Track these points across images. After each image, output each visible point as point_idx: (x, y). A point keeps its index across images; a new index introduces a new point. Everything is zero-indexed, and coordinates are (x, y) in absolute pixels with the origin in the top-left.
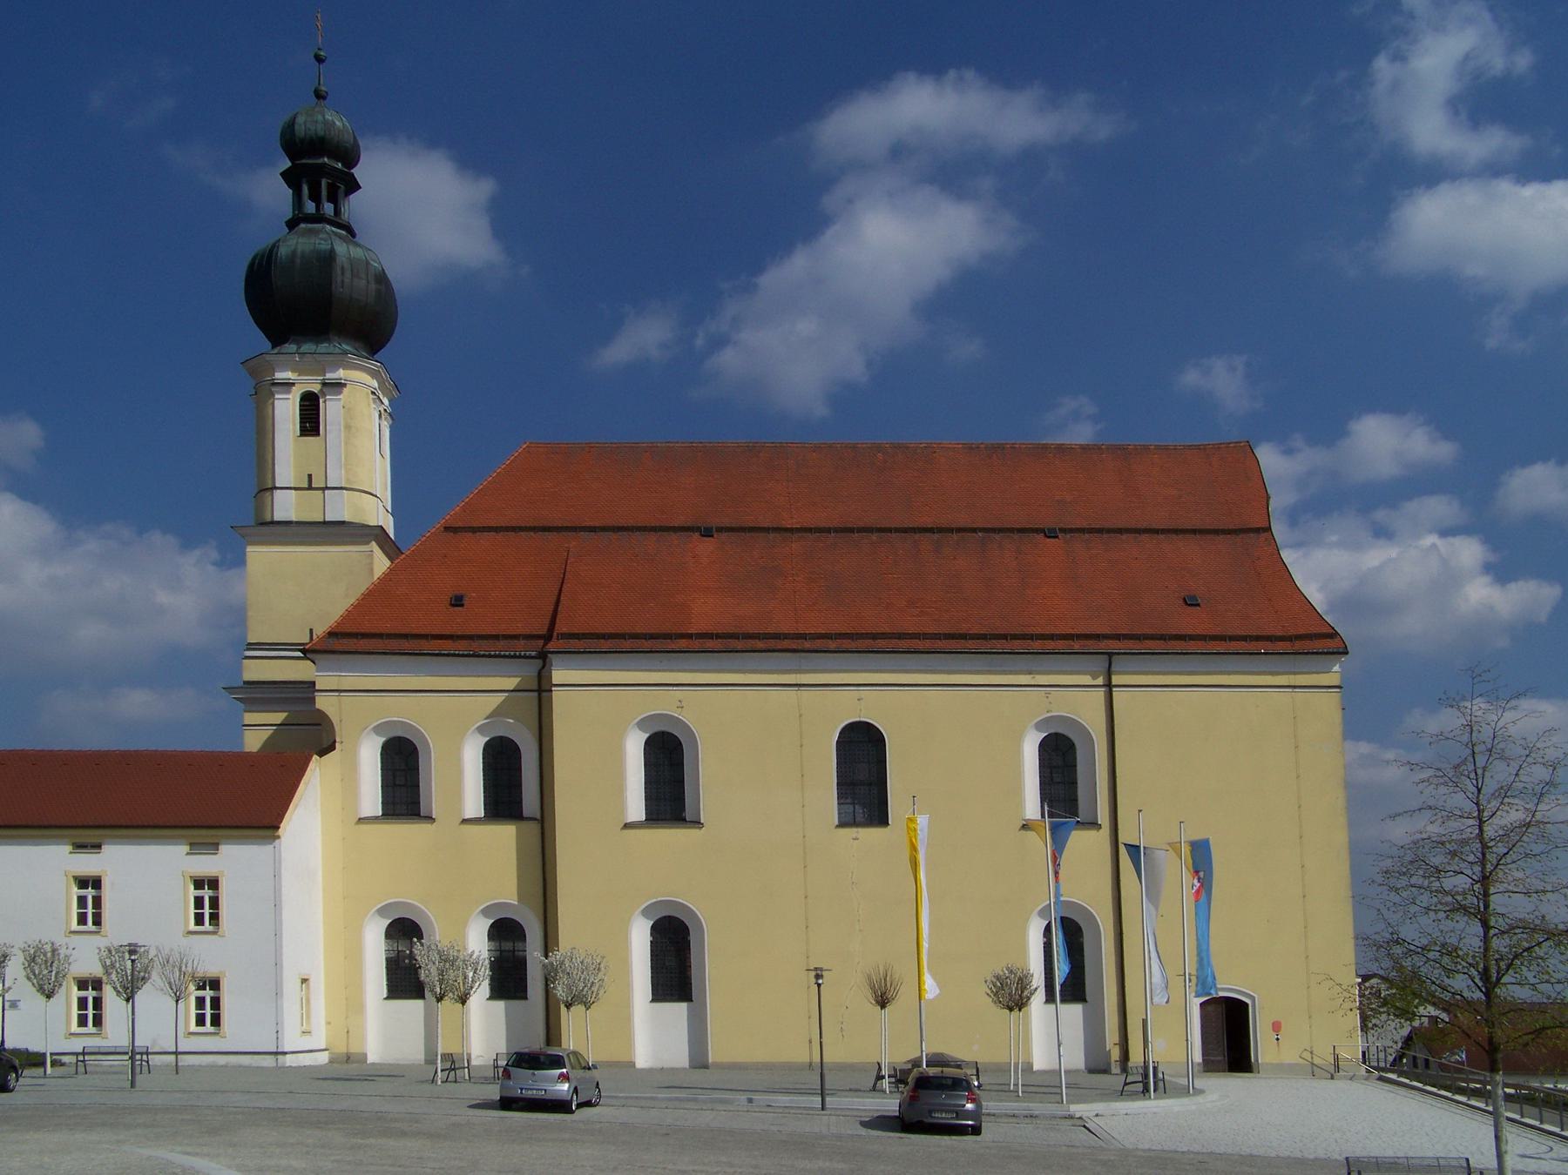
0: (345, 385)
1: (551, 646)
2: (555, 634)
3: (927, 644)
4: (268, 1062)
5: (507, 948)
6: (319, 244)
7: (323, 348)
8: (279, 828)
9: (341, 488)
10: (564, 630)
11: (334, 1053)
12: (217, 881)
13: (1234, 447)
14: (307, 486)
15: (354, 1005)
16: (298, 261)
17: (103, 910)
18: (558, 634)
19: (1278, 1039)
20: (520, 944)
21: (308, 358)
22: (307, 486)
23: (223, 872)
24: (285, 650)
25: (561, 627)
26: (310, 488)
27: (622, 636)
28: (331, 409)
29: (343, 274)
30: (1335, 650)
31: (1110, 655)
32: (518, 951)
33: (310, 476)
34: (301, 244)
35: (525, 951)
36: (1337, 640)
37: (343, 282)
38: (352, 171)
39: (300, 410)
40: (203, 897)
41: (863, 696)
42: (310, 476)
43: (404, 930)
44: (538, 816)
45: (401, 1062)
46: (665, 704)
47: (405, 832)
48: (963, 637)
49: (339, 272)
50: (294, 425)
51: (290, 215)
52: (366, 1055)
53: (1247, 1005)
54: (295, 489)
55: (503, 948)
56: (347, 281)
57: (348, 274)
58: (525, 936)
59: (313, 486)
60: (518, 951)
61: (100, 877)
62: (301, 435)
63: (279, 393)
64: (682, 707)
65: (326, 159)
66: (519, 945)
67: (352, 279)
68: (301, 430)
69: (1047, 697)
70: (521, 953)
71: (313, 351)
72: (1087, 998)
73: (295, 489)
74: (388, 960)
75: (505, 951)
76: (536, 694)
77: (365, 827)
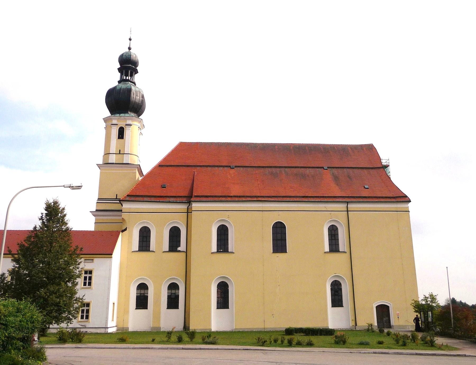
0: (132, 125)
1: (192, 199)
2: (193, 196)
3: (300, 199)
4: (102, 331)
5: (173, 292)
6: (128, 87)
7: (127, 115)
8: (112, 254)
9: (128, 154)
10: (196, 195)
11: (118, 328)
12: (92, 271)
13: (240, 145)
14: (119, 153)
15: (126, 312)
16: (121, 91)
17: (92, 281)
18: (194, 196)
19: (398, 317)
20: (177, 291)
21: (122, 118)
22: (119, 153)
23: (94, 268)
24: (112, 200)
25: (195, 194)
26: (120, 153)
27: (243, 197)
28: (127, 133)
29: (133, 95)
30: (407, 201)
31: (348, 202)
32: (177, 293)
33: (120, 150)
34: (123, 86)
35: (179, 293)
36: (407, 198)
37: (133, 97)
38: (137, 68)
39: (119, 132)
40: (87, 277)
41: (280, 214)
42: (120, 150)
43: (143, 287)
44: (185, 251)
45: (138, 330)
46: (224, 216)
47: (144, 254)
48: (307, 197)
49: (133, 94)
50: (117, 136)
51: (119, 80)
52: (129, 328)
53: (389, 307)
54: (115, 154)
55: (172, 292)
56: (135, 97)
57: (135, 95)
58: (148, 289)
59: (121, 153)
60: (177, 293)
61: (92, 270)
62: (118, 139)
63: (113, 127)
64: (229, 217)
65: (130, 65)
66: (177, 291)
67: (136, 97)
68: (118, 137)
69: (330, 214)
70: (177, 294)
71: (123, 116)
72: (344, 306)
73: (115, 154)
74: (137, 297)
75: (142, 294)
76: (349, 210)
77: (165, 253)
